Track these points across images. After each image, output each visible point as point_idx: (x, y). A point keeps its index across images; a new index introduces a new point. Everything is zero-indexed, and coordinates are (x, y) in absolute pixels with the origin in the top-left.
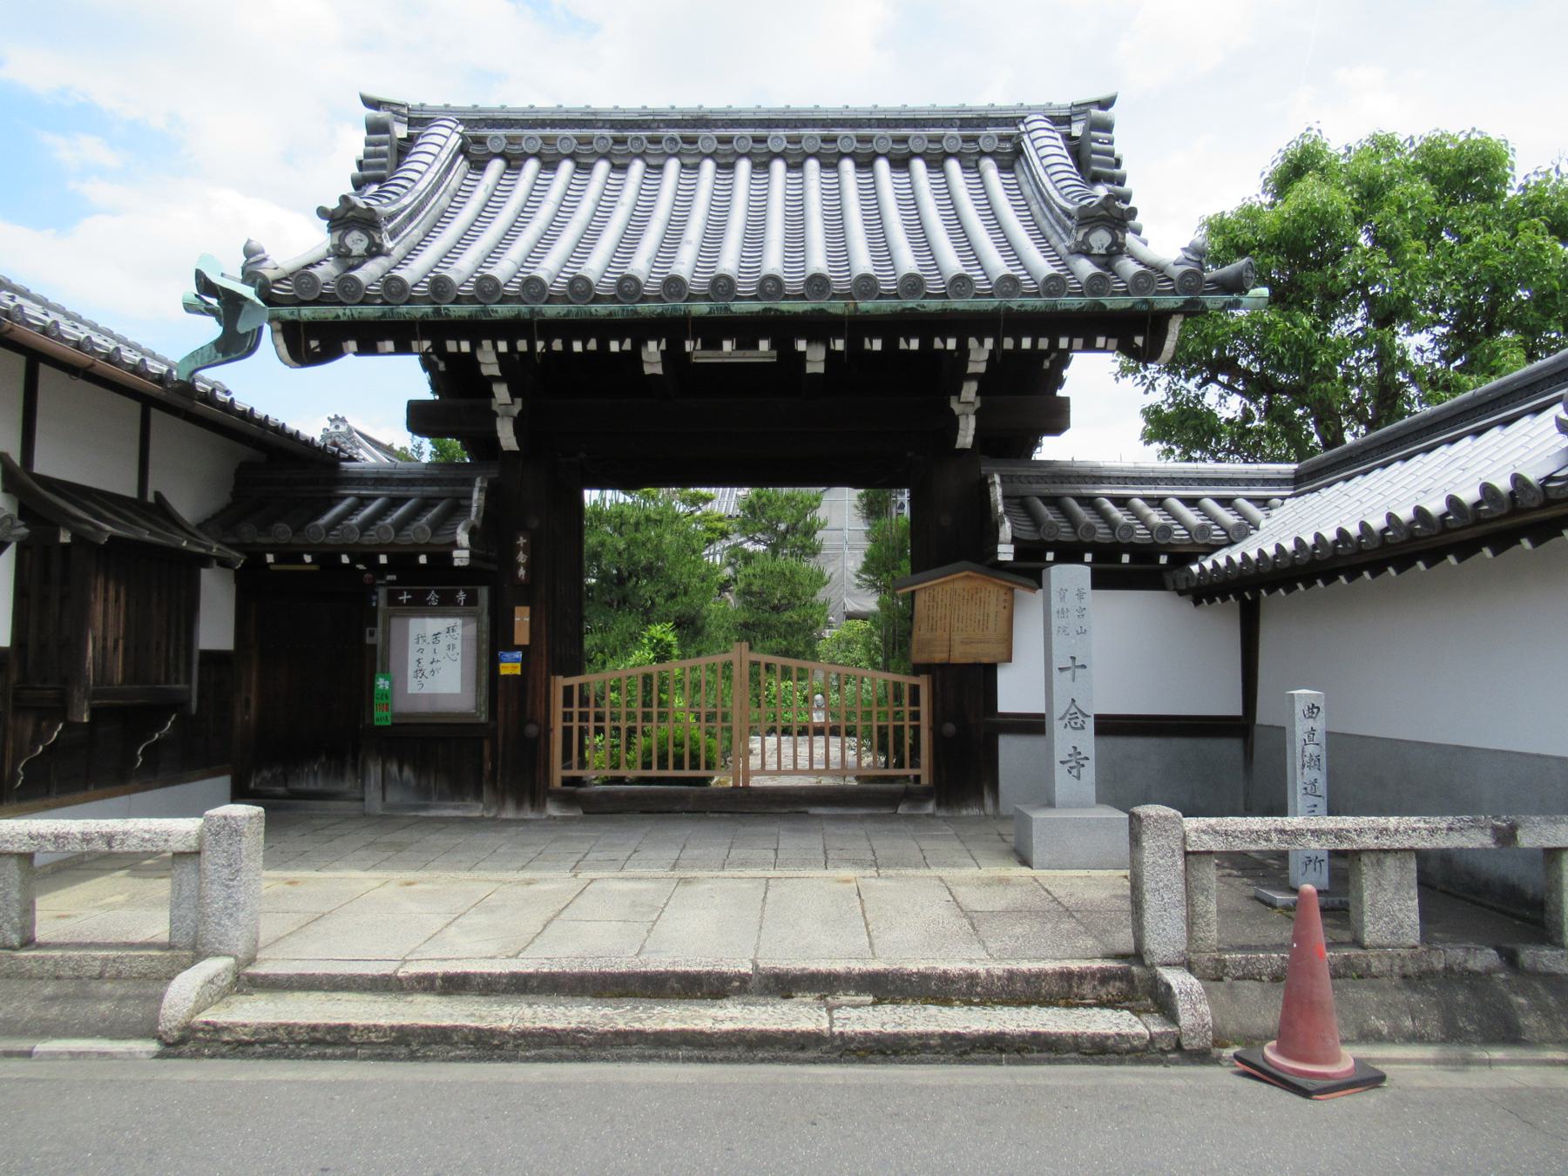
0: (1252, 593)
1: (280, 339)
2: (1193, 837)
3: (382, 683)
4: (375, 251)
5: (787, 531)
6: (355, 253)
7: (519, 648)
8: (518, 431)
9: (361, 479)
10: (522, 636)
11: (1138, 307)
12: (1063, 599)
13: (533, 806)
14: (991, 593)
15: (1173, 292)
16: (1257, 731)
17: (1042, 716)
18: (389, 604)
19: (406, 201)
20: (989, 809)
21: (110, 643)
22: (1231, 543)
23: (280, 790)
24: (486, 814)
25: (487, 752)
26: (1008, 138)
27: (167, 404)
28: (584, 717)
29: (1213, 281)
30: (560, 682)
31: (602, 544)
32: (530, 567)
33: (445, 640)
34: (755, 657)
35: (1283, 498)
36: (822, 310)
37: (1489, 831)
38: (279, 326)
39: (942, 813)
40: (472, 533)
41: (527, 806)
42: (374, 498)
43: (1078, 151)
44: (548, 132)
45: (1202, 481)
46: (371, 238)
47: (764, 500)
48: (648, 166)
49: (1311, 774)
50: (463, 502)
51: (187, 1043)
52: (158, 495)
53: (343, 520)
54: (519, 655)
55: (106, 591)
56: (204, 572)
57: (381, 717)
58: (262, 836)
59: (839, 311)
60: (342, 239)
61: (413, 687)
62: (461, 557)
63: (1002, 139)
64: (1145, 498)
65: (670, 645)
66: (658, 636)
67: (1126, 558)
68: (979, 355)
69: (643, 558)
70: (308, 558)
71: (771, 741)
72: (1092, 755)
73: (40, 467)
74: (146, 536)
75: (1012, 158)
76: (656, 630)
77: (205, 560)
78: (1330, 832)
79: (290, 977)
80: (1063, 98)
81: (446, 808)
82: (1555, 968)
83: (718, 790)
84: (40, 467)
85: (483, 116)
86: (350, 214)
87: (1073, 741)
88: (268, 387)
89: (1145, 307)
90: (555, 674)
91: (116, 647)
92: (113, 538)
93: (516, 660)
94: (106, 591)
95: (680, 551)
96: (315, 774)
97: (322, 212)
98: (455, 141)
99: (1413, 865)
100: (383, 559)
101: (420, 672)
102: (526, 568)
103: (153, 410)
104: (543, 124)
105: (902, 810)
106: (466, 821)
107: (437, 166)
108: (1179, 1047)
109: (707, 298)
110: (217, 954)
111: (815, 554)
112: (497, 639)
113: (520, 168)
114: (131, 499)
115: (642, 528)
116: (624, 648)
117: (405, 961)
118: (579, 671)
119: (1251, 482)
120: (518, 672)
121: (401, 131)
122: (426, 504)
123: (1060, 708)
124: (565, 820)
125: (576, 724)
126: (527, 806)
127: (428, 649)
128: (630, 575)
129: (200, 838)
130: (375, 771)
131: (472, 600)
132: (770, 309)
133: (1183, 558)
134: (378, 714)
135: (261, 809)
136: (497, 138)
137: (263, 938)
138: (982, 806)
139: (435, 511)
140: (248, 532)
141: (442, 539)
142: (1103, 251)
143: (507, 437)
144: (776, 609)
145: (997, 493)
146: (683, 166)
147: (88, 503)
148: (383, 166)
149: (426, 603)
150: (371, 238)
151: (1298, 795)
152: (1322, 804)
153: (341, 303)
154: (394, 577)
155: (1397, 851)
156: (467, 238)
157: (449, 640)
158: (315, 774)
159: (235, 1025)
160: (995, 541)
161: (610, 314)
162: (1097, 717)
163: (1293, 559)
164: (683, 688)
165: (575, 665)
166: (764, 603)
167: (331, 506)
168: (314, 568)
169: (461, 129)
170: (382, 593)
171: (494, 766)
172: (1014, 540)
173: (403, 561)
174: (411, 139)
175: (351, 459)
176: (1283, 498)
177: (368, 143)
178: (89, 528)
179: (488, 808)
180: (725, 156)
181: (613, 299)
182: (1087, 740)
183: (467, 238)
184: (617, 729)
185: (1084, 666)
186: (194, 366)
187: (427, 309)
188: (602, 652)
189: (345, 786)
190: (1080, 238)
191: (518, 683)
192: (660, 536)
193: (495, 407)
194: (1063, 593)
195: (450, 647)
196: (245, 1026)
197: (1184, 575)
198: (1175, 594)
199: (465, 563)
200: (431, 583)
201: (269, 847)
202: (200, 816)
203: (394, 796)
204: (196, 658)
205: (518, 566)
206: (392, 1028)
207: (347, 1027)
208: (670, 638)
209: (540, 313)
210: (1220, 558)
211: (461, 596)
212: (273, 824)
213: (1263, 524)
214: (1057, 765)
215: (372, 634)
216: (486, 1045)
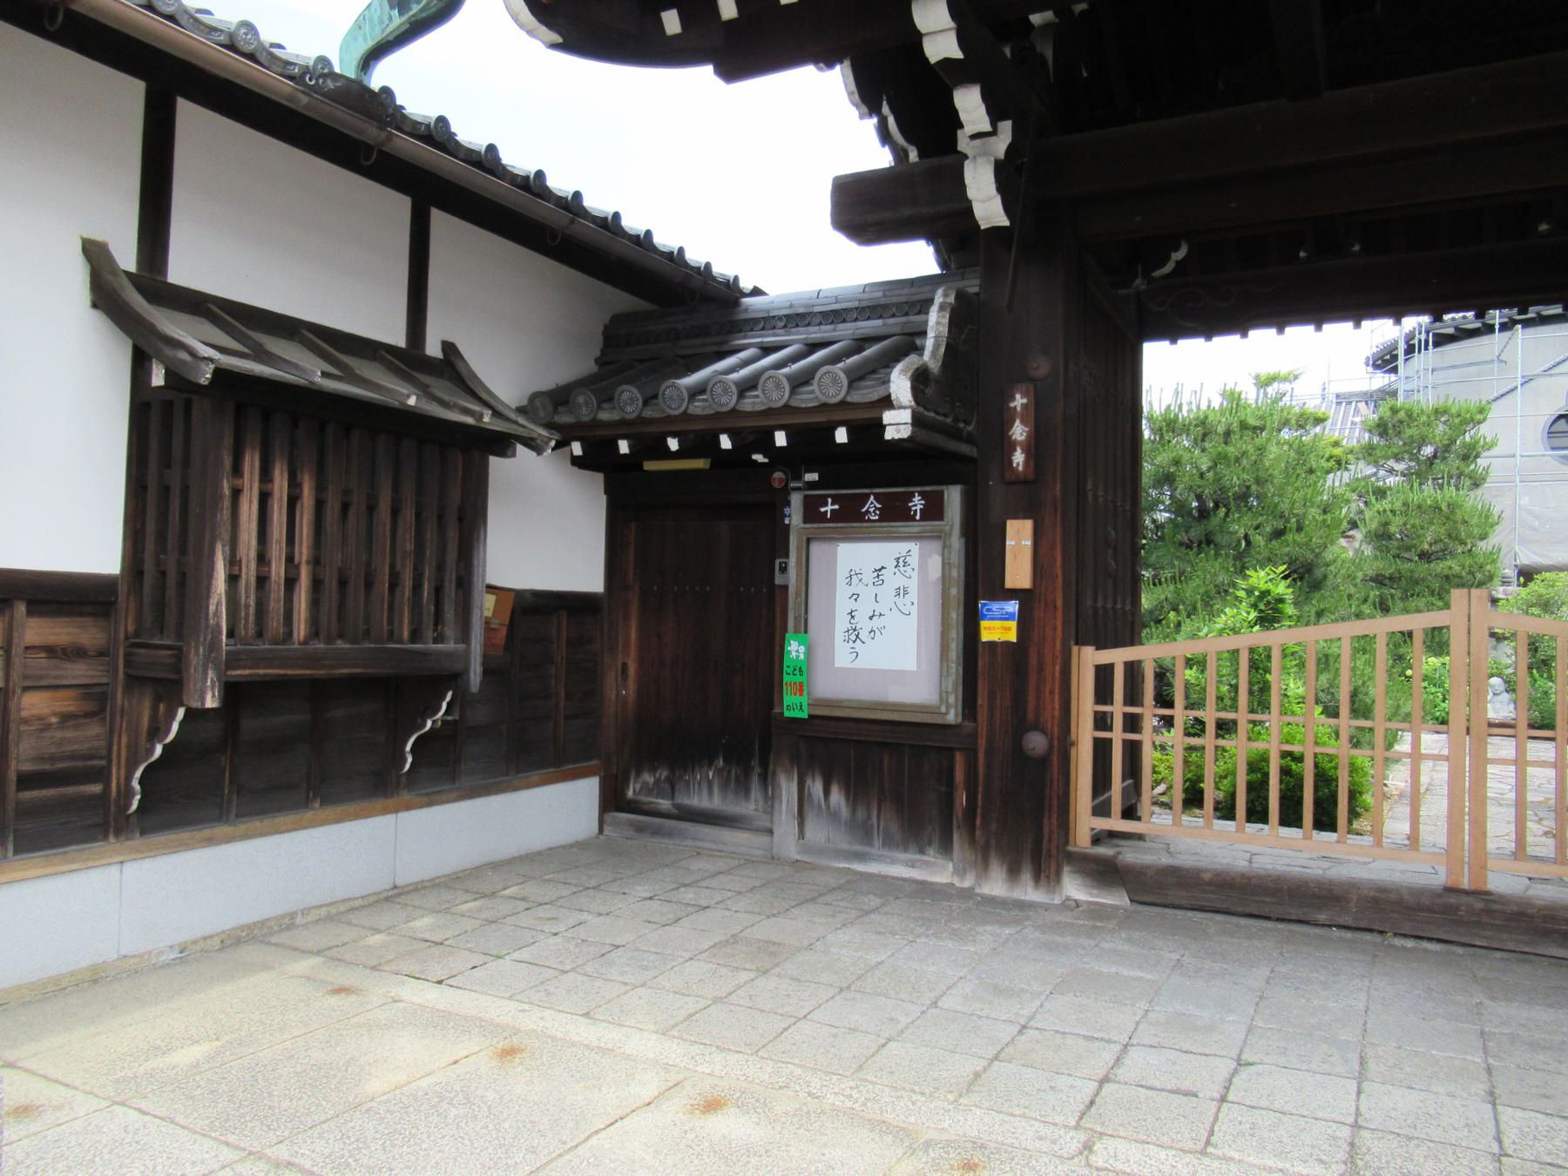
3: (794, 649)
5: (1435, 456)
9: (767, 321)
10: (1019, 573)
13: (1037, 878)
18: (807, 519)
21: (277, 570)
23: (664, 804)
25: (959, 775)
30: (1089, 658)
31: (1177, 462)
32: (1035, 448)
33: (893, 580)
40: (920, 379)
41: (1027, 877)
47: (1402, 415)
50: (918, 342)
52: (449, 348)
54: (1013, 606)
55: (266, 475)
57: (794, 706)
61: (842, 657)
62: (897, 424)
65: (1281, 600)
66: (1263, 587)
69: (1235, 479)
73: (182, 271)
76: (1259, 578)
81: (893, 862)
83: (944, 365)
84: (182, 271)
92: (220, 374)
93: (1008, 617)
94: (266, 475)
95: (1290, 471)
101: (854, 634)
102: (1027, 451)
106: (925, 890)
111: (1476, 485)
112: (979, 577)
115: (1234, 438)
116: (1207, 604)
118: (1130, 637)
120: (1012, 637)
124: (1098, 913)
125: (1117, 736)
126: (1027, 877)
127: (867, 593)
128: (1217, 506)
130: (788, 788)
134: (788, 699)
143: (988, 208)
144: (1424, 556)
149: (861, 517)
157: (900, 581)
164: (1302, 665)
165: (1124, 627)
166: (1408, 549)
170: (796, 500)
173: (811, 442)
178: (184, 356)
184: (1199, 722)
188: (1176, 609)
189: (749, 807)
191: (1015, 654)
192: (1261, 450)
195: (901, 592)
199: (905, 433)
200: (867, 477)
203: (817, 832)
205: (1011, 446)
208: (1281, 588)
211: (917, 503)
215: (784, 569)
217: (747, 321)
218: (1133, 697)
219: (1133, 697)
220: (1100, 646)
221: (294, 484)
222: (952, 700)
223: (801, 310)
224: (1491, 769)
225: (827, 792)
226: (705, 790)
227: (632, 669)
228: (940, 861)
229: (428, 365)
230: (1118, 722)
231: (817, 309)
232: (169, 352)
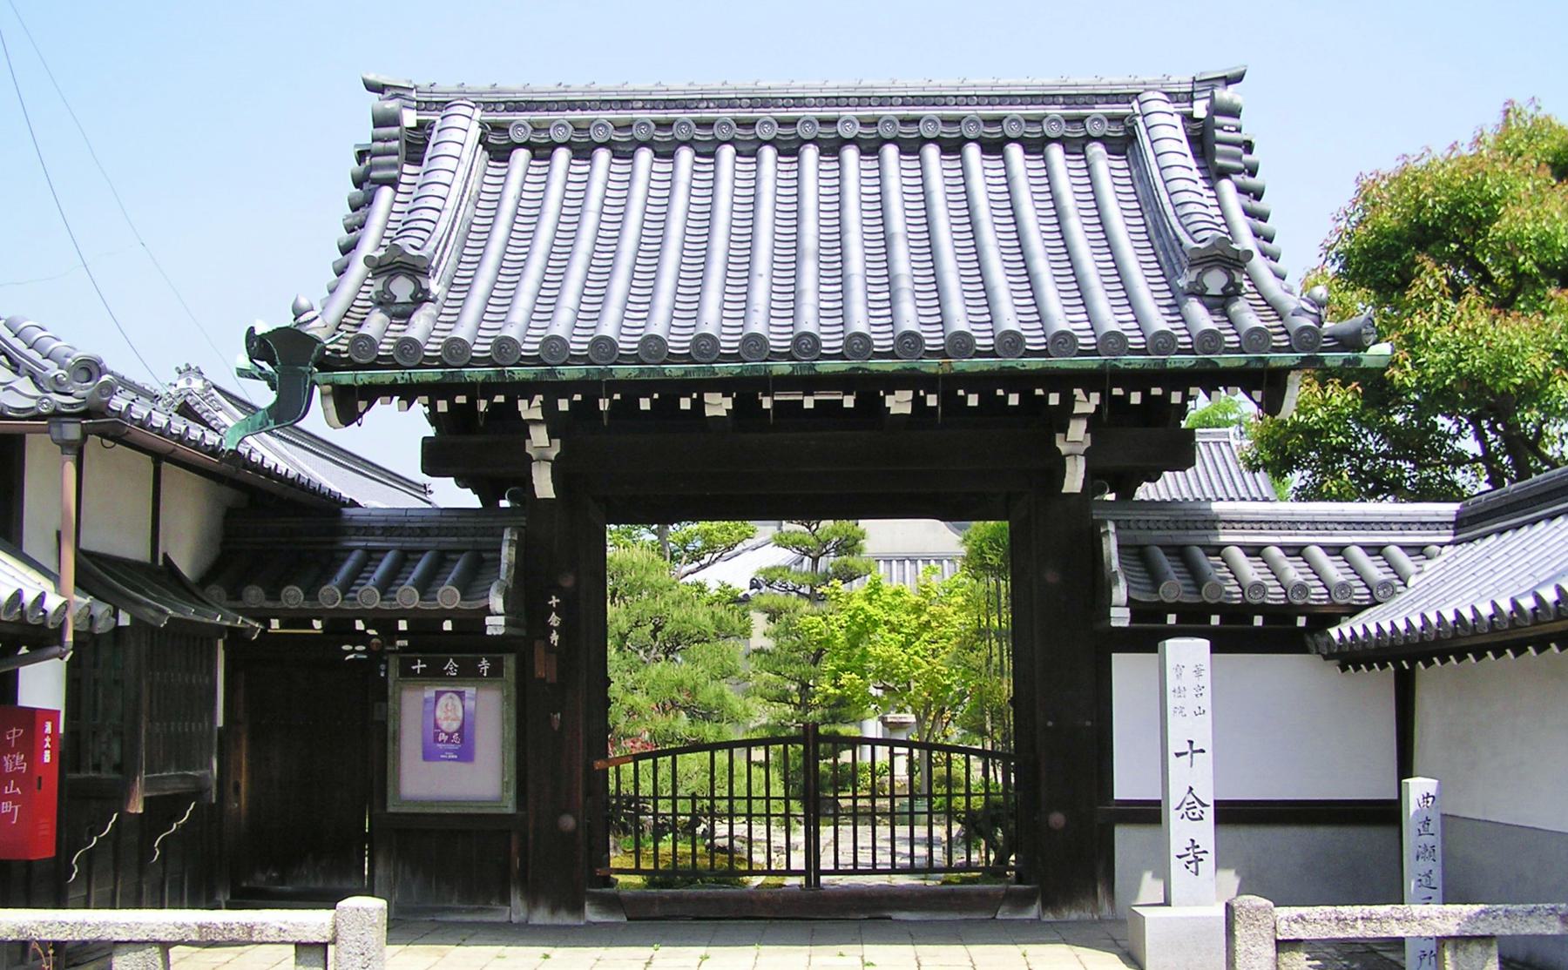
0: (1406, 659)
1: (331, 404)
6: (398, 300)
11: (1253, 365)
15: (1290, 349)
17: (1158, 803)
20: (1106, 910)
26: (1120, 119)
29: (1333, 337)
35: (1442, 545)
39: (1049, 917)
42: (386, 551)
43: (1201, 140)
44: (577, 115)
46: (418, 284)
49: (1425, 865)
60: (386, 285)
62: (495, 625)
63: (1112, 119)
67: (1258, 621)
68: (1087, 403)
72: (1211, 849)
75: (1124, 143)
87: (1189, 830)
89: (1260, 365)
99: (1494, 951)
100: (403, 625)
103: (164, 464)
104: (571, 105)
109: (788, 356)
113: (549, 157)
114: (138, 565)
119: (1406, 525)
121: (410, 119)
123: (1176, 795)
130: (396, 398)
131: (496, 671)
133: (1324, 618)
138: (1096, 908)
143: (544, 485)
145: (1111, 546)
146: (738, 154)
148: (394, 166)
150: (418, 284)
153: (397, 366)
154: (405, 643)
156: (509, 271)
163: (1422, 636)
167: (339, 567)
169: (478, 114)
170: (394, 661)
171: (524, 863)
172: (1131, 602)
175: (353, 504)
181: (688, 358)
182: (1205, 832)
183: (509, 271)
197: (1325, 639)
200: (450, 649)
211: (485, 665)
224: (708, 754)
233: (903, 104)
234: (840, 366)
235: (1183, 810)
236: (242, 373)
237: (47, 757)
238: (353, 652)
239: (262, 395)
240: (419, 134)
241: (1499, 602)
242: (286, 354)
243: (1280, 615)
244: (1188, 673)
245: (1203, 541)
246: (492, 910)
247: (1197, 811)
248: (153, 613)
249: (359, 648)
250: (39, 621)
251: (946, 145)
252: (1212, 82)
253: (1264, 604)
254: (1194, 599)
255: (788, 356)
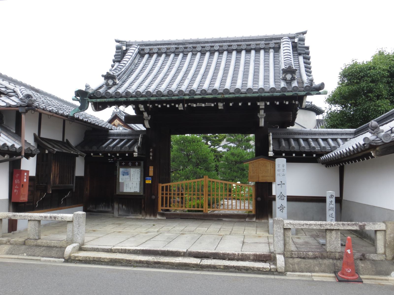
1: (93, 106)
2: (286, 225)
4: (115, 84)
7: (150, 176)
8: (149, 124)
9: (113, 135)
10: (151, 173)
12: (279, 167)
14: (268, 163)
15: (303, 91)
16: (343, 201)
19: (123, 70)
21: (56, 175)
22: (332, 151)
23: (95, 210)
24: (142, 218)
25: (143, 202)
26: (278, 43)
27: (68, 121)
28: (166, 194)
30: (160, 185)
34: (210, 180)
35: (351, 138)
36: (216, 97)
37: (358, 226)
38: (93, 103)
39: (257, 221)
40: (138, 148)
43: (295, 47)
44: (159, 47)
45: (329, 134)
46: (114, 81)
48: (184, 54)
50: (137, 140)
51: (69, 260)
52: (67, 140)
53: (110, 144)
55: (55, 164)
56: (77, 158)
58: (85, 218)
59: (220, 98)
60: (107, 81)
62: (136, 154)
63: (275, 43)
64: (312, 139)
70: (100, 154)
71: (234, 201)
72: (286, 206)
73: (42, 136)
74: (64, 151)
77: (77, 156)
78: (319, 225)
79: (90, 248)
80: (293, 32)
82: (374, 258)
85: (144, 43)
86: (109, 75)
88: (91, 114)
89: (296, 95)
90: (159, 183)
91: (57, 176)
92: (57, 152)
94: (55, 164)
96: (103, 207)
97: (103, 76)
98: (137, 50)
100: (118, 155)
105: (247, 220)
107: (132, 58)
108: (277, 271)
109: (188, 95)
110: (75, 243)
112: (145, 175)
117: (114, 246)
118: (169, 181)
119: (342, 134)
120: (150, 182)
121: (124, 48)
122: (129, 141)
125: (164, 196)
129: (73, 219)
130: (116, 206)
132: (203, 97)
135: (85, 213)
136: (147, 49)
137: (85, 241)
139: (130, 143)
140: (87, 148)
141: (131, 150)
142: (290, 79)
145: (271, 138)
147: (51, 143)
150: (114, 81)
151: (328, 218)
152: (334, 219)
154: (121, 159)
155: (335, 230)
158: (103, 207)
159: (79, 256)
160: (268, 151)
161: (166, 99)
162: (287, 196)
168: (103, 156)
170: (118, 162)
173: (122, 154)
174: (127, 50)
176: (351, 138)
177: (116, 52)
179: (143, 216)
180: (204, 51)
182: (285, 203)
185: (284, 184)
186: (74, 113)
187: (125, 99)
190: (284, 76)
193: (144, 118)
194: (279, 165)
196: (81, 257)
198: (321, 164)
200: (128, 161)
201: (86, 222)
202: (73, 213)
203: (120, 213)
204: (75, 178)
206: (109, 258)
207: (100, 258)
209: (150, 99)
210: (330, 155)
211: (137, 164)
212: (88, 217)
213: (341, 146)
214: (277, 209)
216: (128, 263)
217: (110, 134)
218: (167, 190)
219: (167, 190)
220: (162, 184)
221: (58, 164)
222: (142, 191)
223: (119, 134)
225: (122, 206)
226: (102, 208)
227: (88, 188)
228: (140, 215)
229: (65, 143)
230: (164, 194)
231: (122, 134)
232: (49, 149)
233: (229, 42)
234: (200, 97)
235: (279, 197)
236: (73, 100)
237: (25, 180)
238: (111, 160)
239: (78, 104)
240: (125, 51)
241: (343, 150)
242: (82, 95)
243: (309, 154)
244: (281, 166)
245: (292, 137)
246: (138, 216)
247: (283, 198)
248: (52, 150)
249: (112, 160)
250: (15, 151)
251: (238, 51)
252: (300, 33)
253: (305, 151)
254: (279, 150)
255: (188, 95)
